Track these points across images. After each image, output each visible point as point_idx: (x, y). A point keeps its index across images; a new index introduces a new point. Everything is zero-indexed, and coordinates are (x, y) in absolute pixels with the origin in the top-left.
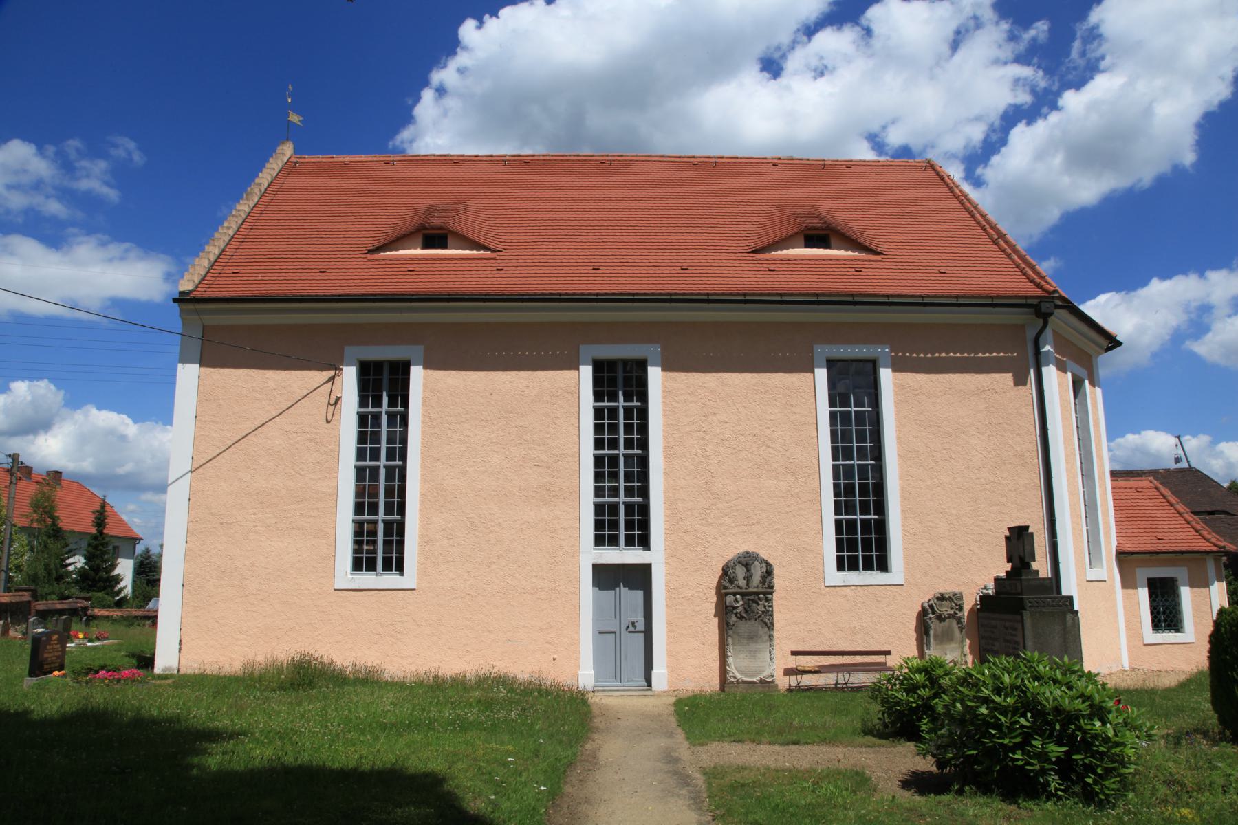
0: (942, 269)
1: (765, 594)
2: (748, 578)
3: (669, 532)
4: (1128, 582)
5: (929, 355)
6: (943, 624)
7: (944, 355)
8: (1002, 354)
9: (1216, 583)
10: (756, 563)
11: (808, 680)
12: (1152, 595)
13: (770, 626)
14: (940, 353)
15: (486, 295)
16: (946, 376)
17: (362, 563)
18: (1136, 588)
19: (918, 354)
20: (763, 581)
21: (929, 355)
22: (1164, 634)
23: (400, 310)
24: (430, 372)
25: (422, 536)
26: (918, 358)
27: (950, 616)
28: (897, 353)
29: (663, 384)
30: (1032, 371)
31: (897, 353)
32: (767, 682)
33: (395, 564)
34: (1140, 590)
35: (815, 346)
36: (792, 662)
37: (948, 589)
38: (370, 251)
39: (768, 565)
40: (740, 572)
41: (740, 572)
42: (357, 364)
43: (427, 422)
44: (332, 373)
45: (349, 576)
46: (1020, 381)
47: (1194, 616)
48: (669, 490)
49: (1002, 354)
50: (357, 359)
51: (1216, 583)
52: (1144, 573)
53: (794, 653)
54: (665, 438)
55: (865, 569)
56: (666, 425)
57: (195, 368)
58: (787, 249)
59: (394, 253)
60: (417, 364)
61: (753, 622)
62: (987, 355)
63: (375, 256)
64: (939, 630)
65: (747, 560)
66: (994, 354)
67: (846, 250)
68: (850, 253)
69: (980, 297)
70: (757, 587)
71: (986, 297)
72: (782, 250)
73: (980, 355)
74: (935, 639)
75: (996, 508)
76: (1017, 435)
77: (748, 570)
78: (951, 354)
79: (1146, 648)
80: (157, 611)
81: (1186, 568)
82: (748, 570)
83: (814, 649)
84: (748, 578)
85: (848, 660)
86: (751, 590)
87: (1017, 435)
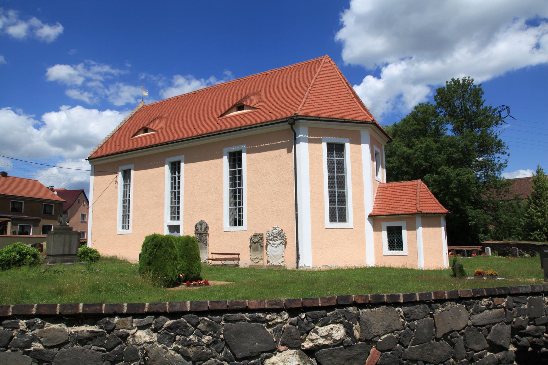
0: (218, 122)
1: (205, 234)
2: (201, 229)
3: (185, 215)
4: (376, 228)
5: (259, 146)
6: (255, 244)
7: (263, 145)
8: (283, 141)
9: (420, 228)
10: (204, 224)
11: (229, 263)
12: (389, 234)
13: (206, 244)
14: (265, 144)
15: (165, 143)
16: (264, 153)
17: (333, 219)
18: (381, 231)
19: (260, 145)
20: (205, 230)
21: (259, 146)
22: (396, 251)
23: (102, 160)
24: (135, 171)
25: (133, 219)
26: (255, 148)
27: (257, 242)
28: (248, 147)
29: (185, 168)
30: (294, 146)
31: (248, 147)
32: (204, 263)
33: (240, 223)
34: (383, 232)
35: (224, 149)
36: (211, 256)
37: (258, 232)
38: (220, 117)
39: (207, 224)
40: (199, 227)
41: (199, 227)
42: (228, 155)
43: (134, 186)
44: (116, 175)
45: (328, 224)
46: (289, 151)
47: (408, 243)
48: (248, 197)
49: (283, 141)
50: (228, 152)
51: (420, 228)
52: (385, 224)
53: (212, 253)
54: (185, 185)
55: (239, 225)
56: (185, 181)
57: (93, 177)
58: (230, 113)
59: (137, 136)
60: (244, 153)
61: (201, 243)
62: (278, 142)
63: (133, 138)
64: (254, 247)
65: (201, 223)
66: (281, 142)
67: (248, 110)
68: (249, 110)
69: (269, 121)
70: (203, 232)
71: (272, 121)
72: (228, 114)
73: (276, 143)
74: (253, 250)
75: (278, 201)
76: (287, 172)
77: (201, 226)
78: (266, 144)
79: (384, 257)
80: (87, 240)
81: (405, 222)
82: (201, 226)
83: (220, 252)
84: (201, 229)
85: (228, 256)
86: (201, 233)
87: (287, 172)
